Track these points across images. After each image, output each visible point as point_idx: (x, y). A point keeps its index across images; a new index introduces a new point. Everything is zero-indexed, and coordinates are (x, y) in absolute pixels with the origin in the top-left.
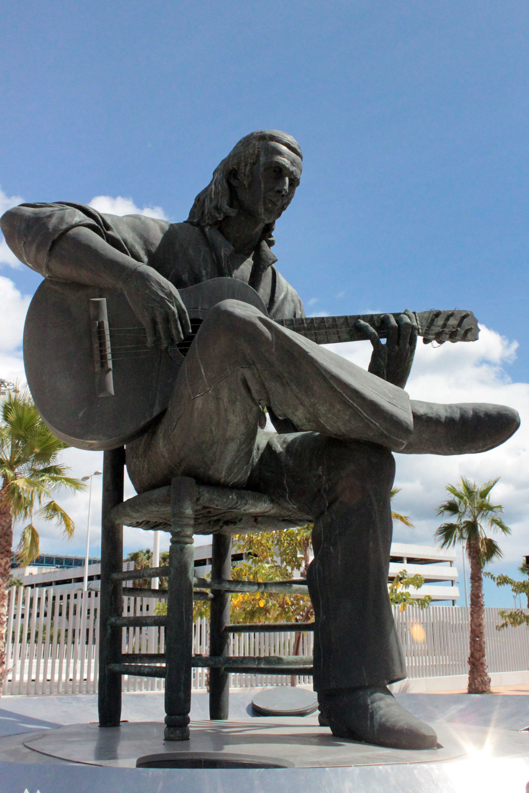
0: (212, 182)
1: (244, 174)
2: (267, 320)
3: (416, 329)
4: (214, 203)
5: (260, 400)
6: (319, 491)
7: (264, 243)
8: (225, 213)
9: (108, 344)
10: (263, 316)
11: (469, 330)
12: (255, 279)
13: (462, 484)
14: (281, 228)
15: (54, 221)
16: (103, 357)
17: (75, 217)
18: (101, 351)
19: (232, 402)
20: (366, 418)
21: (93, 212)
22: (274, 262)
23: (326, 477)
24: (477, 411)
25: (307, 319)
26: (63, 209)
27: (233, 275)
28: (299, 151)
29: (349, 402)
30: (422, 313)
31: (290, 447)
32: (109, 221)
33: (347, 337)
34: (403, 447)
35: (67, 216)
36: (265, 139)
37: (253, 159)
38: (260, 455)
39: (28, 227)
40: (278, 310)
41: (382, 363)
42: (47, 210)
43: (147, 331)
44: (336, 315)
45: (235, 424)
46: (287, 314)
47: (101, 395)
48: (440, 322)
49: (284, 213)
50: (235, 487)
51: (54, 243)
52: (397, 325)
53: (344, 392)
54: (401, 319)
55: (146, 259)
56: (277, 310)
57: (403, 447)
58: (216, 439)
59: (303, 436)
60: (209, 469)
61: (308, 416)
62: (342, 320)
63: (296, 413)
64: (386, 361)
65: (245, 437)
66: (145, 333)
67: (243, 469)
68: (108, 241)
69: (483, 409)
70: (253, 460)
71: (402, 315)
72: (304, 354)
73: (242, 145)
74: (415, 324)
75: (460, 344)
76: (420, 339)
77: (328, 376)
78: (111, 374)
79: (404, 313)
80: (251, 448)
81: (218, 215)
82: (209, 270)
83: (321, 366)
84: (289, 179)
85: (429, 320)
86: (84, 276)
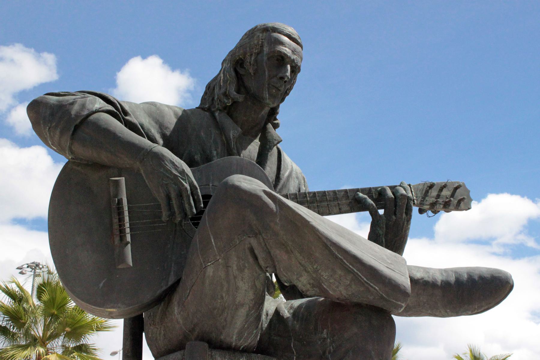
0: (220, 71)
1: (250, 63)
2: (271, 193)
3: (411, 199)
4: (223, 90)
5: (267, 268)
6: (324, 353)
7: (270, 126)
8: (233, 99)
9: (127, 219)
10: (267, 189)
11: (462, 199)
12: (262, 158)
13: (469, 352)
14: (286, 112)
15: (76, 108)
16: (122, 231)
17: (95, 104)
18: (120, 226)
19: (241, 270)
20: (366, 282)
21: (112, 99)
22: (279, 142)
23: (330, 339)
24: (472, 274)
25: (309, 193)
26: (84, 97)
27: (242, 155)
28: (299, 41)
29: (350, 268)
30: (417, 185)
31: (296, 313)
32: (127, 108)
33: (348, 208)
34: (402, 309)
35: (88, 102)
36: (268, 30)
37: (258, 49)
38: (269, 320)
39: (52, 115)
40: (284, 186)
41: (381, 232)
42: (70, 98)
43: (162, 206)
44: (336, 189)
45: (244, 291)
46: (292, 189)
47: (120, 267)
48: (434, 193)
49: (287, 98)
50: (245, 351)
51: (77, 128)
52: (393, 196)
53: (344, 258)
54: (397, 191)
55: (161, 142)
56: (282, 186)
57: (402, 309)
58: (226, 304)
59: (309, 301)
60: (221, 333)
61: (312, 281)
62: (343, 193)
63: (300, 279)
64: (385, 229)
65: (253, 303)
66: (161, 209)
67: (253, 334)
68: (126, 126)
69: (477, 272)
70: (262, 325)
71: (398, 187)
72: (306, 223)
73: (247, 38)
74: (410, 195)
75: (455, 214)
76: (415, 210)
77: (329, 244)
78: (129, 245)
79: (400, 186)
80: (259, 313)
81: (226, 101)
82: (219, 150)
83: (322, 234)
84: (291, 67)
85: (424, 191)
86: (104, 157)
